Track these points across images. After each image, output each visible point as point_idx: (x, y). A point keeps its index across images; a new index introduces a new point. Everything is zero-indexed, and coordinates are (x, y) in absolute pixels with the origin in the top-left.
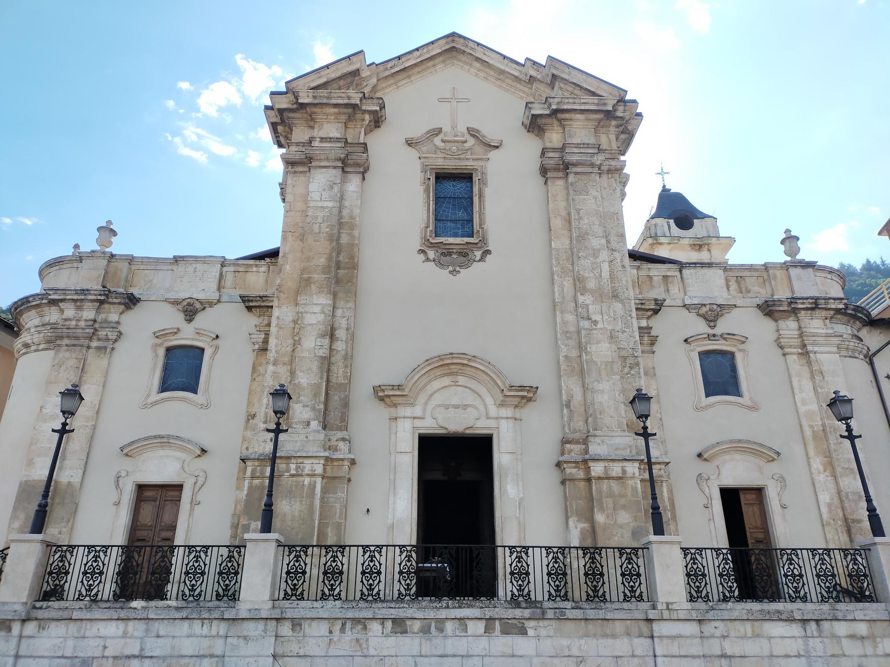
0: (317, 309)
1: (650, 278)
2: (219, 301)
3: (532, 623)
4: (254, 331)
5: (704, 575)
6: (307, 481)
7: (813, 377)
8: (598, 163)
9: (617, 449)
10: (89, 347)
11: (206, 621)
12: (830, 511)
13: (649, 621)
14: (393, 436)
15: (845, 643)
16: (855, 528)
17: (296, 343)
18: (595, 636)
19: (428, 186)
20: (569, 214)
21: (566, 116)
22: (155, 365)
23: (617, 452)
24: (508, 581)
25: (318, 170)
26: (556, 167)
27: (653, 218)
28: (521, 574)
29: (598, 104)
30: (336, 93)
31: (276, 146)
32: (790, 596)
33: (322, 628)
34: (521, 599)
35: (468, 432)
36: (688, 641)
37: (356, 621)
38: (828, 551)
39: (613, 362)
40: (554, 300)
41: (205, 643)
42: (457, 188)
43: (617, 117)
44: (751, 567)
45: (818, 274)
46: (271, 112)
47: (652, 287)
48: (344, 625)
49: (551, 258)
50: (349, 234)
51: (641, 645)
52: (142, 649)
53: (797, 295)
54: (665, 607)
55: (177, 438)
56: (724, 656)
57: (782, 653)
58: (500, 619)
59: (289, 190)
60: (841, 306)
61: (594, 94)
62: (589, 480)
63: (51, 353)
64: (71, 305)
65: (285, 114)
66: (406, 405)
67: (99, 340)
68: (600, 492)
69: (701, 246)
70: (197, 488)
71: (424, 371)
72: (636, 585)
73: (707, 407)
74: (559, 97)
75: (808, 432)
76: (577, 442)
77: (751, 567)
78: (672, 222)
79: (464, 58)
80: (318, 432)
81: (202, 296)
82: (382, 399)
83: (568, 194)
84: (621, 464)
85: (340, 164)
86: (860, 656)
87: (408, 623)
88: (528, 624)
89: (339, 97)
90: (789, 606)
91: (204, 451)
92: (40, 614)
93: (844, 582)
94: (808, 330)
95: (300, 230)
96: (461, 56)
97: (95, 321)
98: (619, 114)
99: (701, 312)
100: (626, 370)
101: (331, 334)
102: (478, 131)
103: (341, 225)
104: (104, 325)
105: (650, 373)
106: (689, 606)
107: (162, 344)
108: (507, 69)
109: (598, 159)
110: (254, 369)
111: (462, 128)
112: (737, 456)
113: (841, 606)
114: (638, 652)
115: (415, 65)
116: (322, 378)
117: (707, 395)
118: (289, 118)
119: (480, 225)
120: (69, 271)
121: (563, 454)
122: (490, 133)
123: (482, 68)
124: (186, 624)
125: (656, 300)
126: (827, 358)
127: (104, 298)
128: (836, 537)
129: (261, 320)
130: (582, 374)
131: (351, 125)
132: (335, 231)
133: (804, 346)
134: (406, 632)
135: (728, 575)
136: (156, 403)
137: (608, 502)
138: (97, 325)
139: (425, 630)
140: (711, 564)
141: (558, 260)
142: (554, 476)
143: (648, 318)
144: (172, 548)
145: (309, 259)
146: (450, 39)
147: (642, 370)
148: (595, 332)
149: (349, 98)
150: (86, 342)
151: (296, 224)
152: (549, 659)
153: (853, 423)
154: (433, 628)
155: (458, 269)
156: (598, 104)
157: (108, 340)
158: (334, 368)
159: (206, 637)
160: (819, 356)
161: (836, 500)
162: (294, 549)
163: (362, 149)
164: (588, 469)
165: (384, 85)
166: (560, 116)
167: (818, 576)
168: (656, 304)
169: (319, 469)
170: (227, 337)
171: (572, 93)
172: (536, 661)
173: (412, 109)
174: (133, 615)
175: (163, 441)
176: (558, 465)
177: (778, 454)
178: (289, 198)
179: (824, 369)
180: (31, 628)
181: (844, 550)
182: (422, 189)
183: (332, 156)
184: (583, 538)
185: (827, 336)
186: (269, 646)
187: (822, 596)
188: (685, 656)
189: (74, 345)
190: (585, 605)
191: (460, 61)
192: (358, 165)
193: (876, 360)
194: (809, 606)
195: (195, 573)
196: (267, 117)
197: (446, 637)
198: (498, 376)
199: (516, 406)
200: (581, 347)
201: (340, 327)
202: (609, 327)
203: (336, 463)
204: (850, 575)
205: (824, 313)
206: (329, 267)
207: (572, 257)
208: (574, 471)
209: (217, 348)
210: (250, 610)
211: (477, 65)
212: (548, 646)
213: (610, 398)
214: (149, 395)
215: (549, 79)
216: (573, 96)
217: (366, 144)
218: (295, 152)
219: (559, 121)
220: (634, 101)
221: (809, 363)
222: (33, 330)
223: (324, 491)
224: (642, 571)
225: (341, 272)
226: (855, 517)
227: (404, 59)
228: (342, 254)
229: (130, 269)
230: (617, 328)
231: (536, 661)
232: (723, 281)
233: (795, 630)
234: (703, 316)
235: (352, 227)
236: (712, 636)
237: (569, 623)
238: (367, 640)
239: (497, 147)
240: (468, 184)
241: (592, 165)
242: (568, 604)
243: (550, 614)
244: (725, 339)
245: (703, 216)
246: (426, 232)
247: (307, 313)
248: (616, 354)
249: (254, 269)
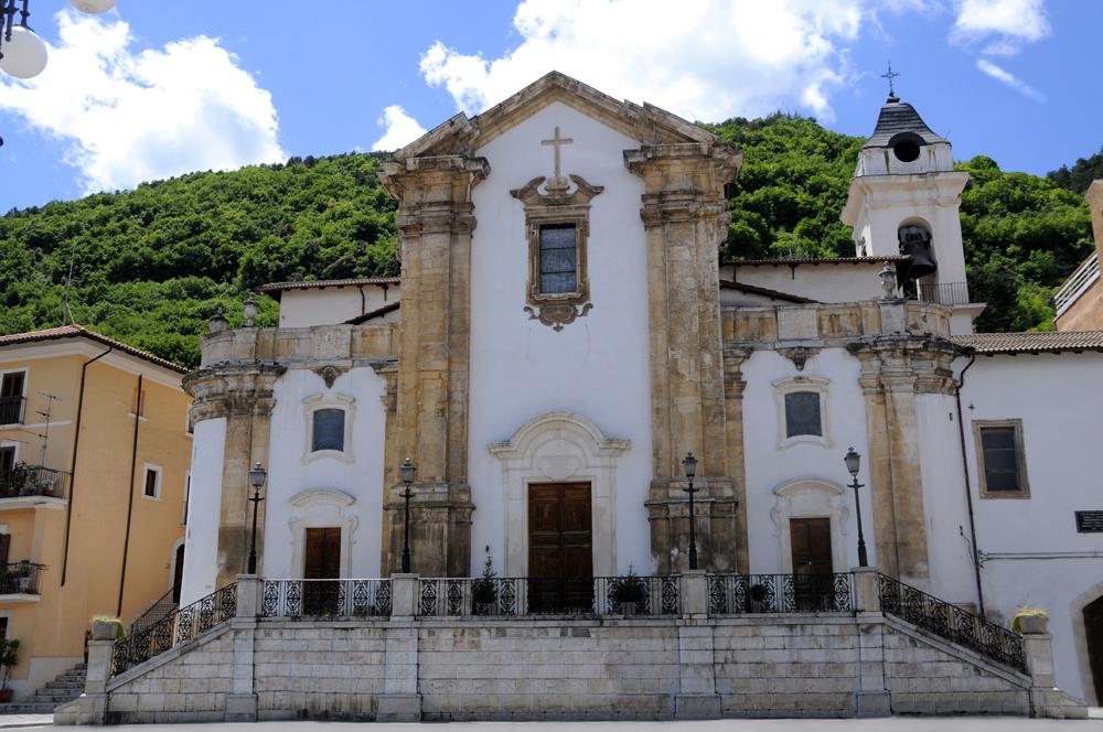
0: (435, 375)
3: (594, 629)
21: (663, 162)
33: (450, 635)
60: (920, 346)
61: (690, 140)
85: (448, 228)
100: (710, 419)
115: (518, 109)
122: (592, 181)
135: (841, 593)
155: (561, 324)
171: (669, 136)
173: (516, 158)
179: (898, 407)
206: (443, 334)
209: (355, 408)
222: (205, 400)
225: (454, 337)
233: (783, 631)
243: (606, 623)
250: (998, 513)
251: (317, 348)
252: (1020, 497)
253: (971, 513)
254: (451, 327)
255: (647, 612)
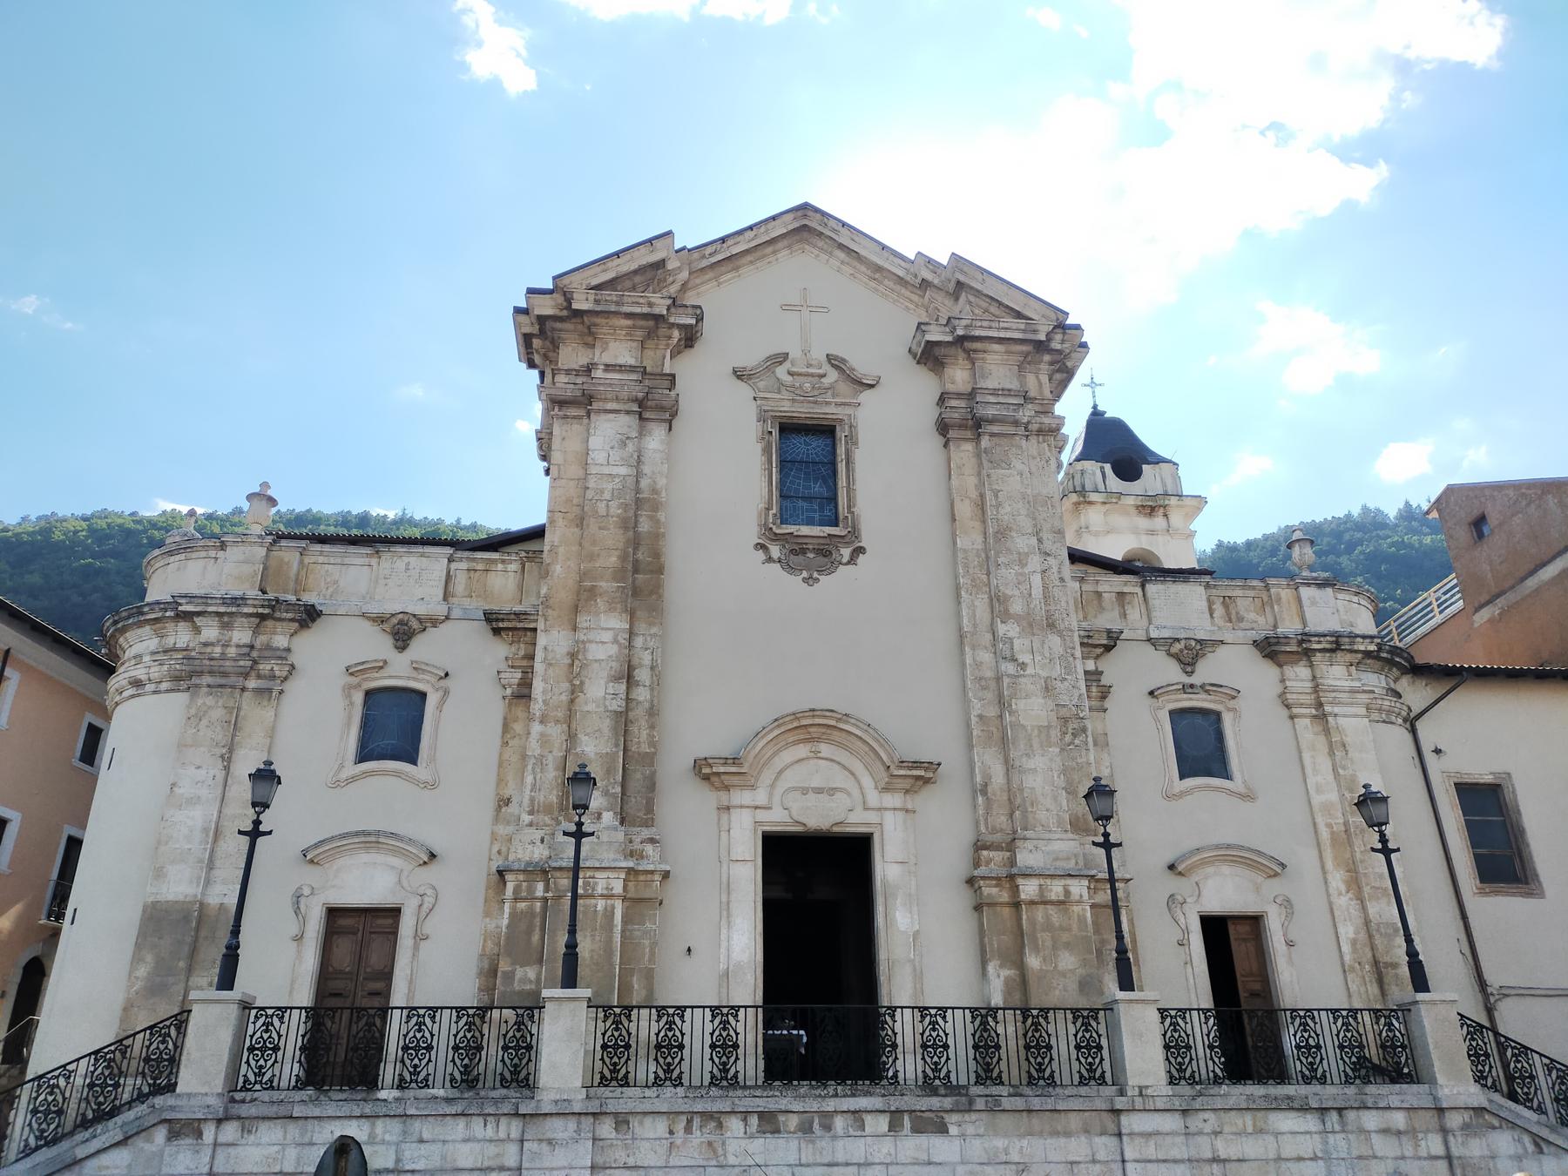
0: (607, 636)
1: (1099, 594)
2: (447, 618)
3: (955, 1117)
4: (503, 666)
5: (1188, 1047)
6: (601, 904)
7: (1331, 753)
8: (1025, 420)
9: (1056, 859)
10: (243, 689)
11: (489, 1119)
12: (1355, 950)
13: (1116, 1112)
14: (724, 835)
15: (1375, 1138)
16: (1389, 975)
17: (575, 691)
18: (1041, 1134)
19: (769, 444)
20: (982, 496)
21: (977, 345)
22: (350, 718)
23: (1058, 864)
24: (919, 1057)
25: (603, 417)
26: (962, 423)
27: (1078, 460)
28: (933, 1046)
29: (1024, 331)
30: (630, 296)
31: (524, 365)
32: (1303, 1076)
33: (660, 1127)
34: (937, 1082)
35: (835, 829)
36: (1169, 1139)
37: (707, 1116)
38: (1354, 1012)
39: (1049, 727)
40: (960, 629)
41: (492, 1150)
42: (815, 445)
43: (1053, 347)
44: (1244, 1034)
45: (1340, 596)
46: (523, 318)
47: (1101, 609)
48: (689, 1122)
49: (955, 563)
50: (651, 518)
51: (1104, 1146)
52: (398, 1160)
53: (1311, 628)
54: (1136, 1092)
55: (393, 835)
56: (1215, 1160)
57: (1294, 1155)
58: (911, 1112)
59: (556, 444)
60: (1372, 648)
61: (1019, 315)
62: (1016, 905)
63: (182, 698)
64: (214, 622)
65: (549, 324)
66: (743, 787)
67: (259, 677)
68: (1032, 922)
69: (1153, 509)
70: (423, 914)
71: (771, 736)
72: (1097, 1065)
73: (1182, 794)
74: (966, 315)
75: (1325, 834)
76: (998, 848)
77: (1244, 1034)
78: (1108, 467)
79: (820, 244)
80: (615, 829)
81: (420, 610)
82: (706, 778)
83: (980, 465)
84: (1063, 882)
85: (635, 408)
86: (1396, 1158)
87: (782, 1118)
88: (952, 1119)
89: (635, 303)
90: (1304, 1090)
91: (433, 856)
92: (244, 1110)
93: (1373, 1053)
94: (1326, 682)
95: (576, 510)
96: (816, 240)
97: (252, 647)
98: (1056, 345)
99: (1173, 650)
100: (1068, 738)
101: (628, 676)
102: (843, 361)
103: (639, 503)
104: (267, 654)
105: (1102, 742)
106: (1169, 1090)
107: (359, 685)
108: (886, 266)
109: (1026, 414)
110: (506, 727)
111: (818, 354)
112: (1226, 869)
113: (1371, 1089)
114: (1101, 1156)
115: (747, 252)
116: (617, 745)
117: (1182, 777)
118: (553, 329)
119: (849, 507)
120: (201, 563)
121: (977, 864)
122: (862, 365)
123: (847, 259)
124: (462, 1122)
125: (1109, 632)
126: (1352, 723)
127: (268, 613)
128: (1363, 989)
129: (513, 649)
130: (1004, 743)
131: (650, 344)
132: (631, 513)
133: (1320, 705)
134: (777, 1131)
136: (353, 779)
137: (1044, 938)
138: (255, 654)
139: (806, 1129)
140: (1200, 1032)
141: (966, 566)
142: (961, 900)
143: (1097, 657)
144: (384, 1011)
145: (592, 557)
146: (799, 213)
147: (1090, 739)
148: (1022, 680)
149: (650, 305)
150: (240, 681)
151: (569, 500)
152: (979, 1168)
153: (1388, 830)
154: (816, 1126)
155: (815, 575)
156: (1024, 331)
157: (273, 677)
158: (634, 729)
159: (491, 1141)
160: (1341, 720)
161: (1363, 936)
162: (614, 1012)
163: (667, 384)
164: (1015, 890)
165: (698, 281)
166: (968, 345)
167: (1341, 1047)
168: (1109, 637)
169: (618, 888)
170: (463, 676)
171: (986, 311)
172: (960, 1169)
174: (384, 1111)
175: (370, 839)
176: (971, 881)
177: (1283, 866)
178: (556, 456)
179: (1348, 740)
180: (230, 1131)
181: (1376, 1011)
182: (759, 447)
183: (624, 395)
184: (1008, 992)
185: (1353, 691)
186: (584, 1154)
187: (1346, 1075)
188: (1164, 1161)
189: (221, 686)
190: (1027, 1091)
191: (815, 246)
192: (662, 409)
193: (1419, 725)
194: (1330, 1090)
195: (417, 1048)
196: (517, 325)
197: (835, 1137)
198: (881, 746)
199: (907, 791)
200: (1002, 703)
201: (641, 666)
202: (1044, 674)
203: (642, 878)
204: (1383, 1046)
205: (1349, 657)
206: (623, 569)
207: (988, 563)
208: (995, 890)
209: (446, 692)
210: (556, 1102)
211: (841, 255)
212: (977, 1148)
213: (1045, 781)
214: (342, 766)
215: (951, 287)
216: (986, 316)
217: (674, 376)
218: (564, 385)
219: (967, 352)
220: (1077, 327)
221: (1327, 731)
222: (147, 658)
223: (626, 920)
224: (1104, 1042)
226: (1387, 959)
227: (730, 242)
228: (642, 549)
229: (301, 562)
230: (1054, 675)
231: (960, 1169)
232: (1205, 604)
233: (1310, 1122)
234: (1177, 657)
235: (656, 507)
236: (1200, 1133)
237: (1004, 1116)
238: (724, 1144)
239: (872, 386)
240: (829, 441)
241: (1016, 423)
242: (1004, 1090)
243: (980, 1104)
244: (1207, 691)
245: (1158, 460)
246: (767, 515)
247: (591, 642)
248: (1053, 716)
249: (500, 566)
250: (1495, 912)
251: (382, 582)
252: (1530, 895)
253: (1464, 917)
254: (636, 563)
255: (1051, 1082)
